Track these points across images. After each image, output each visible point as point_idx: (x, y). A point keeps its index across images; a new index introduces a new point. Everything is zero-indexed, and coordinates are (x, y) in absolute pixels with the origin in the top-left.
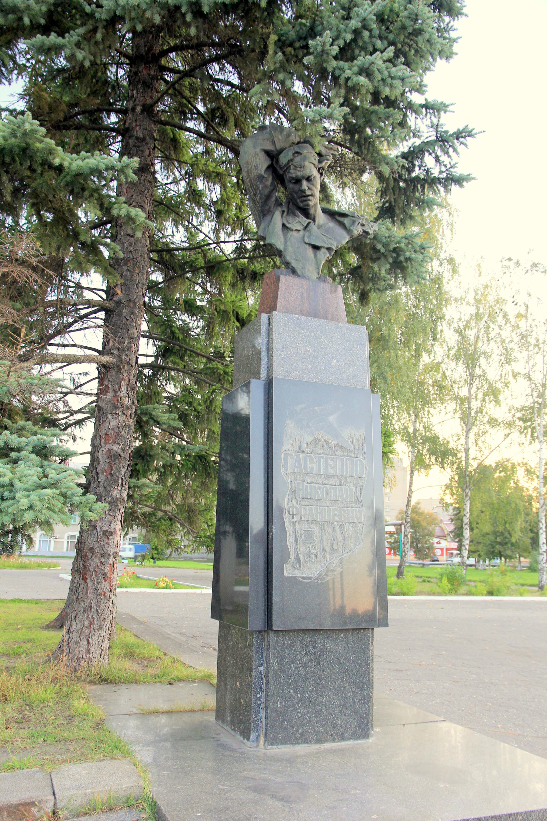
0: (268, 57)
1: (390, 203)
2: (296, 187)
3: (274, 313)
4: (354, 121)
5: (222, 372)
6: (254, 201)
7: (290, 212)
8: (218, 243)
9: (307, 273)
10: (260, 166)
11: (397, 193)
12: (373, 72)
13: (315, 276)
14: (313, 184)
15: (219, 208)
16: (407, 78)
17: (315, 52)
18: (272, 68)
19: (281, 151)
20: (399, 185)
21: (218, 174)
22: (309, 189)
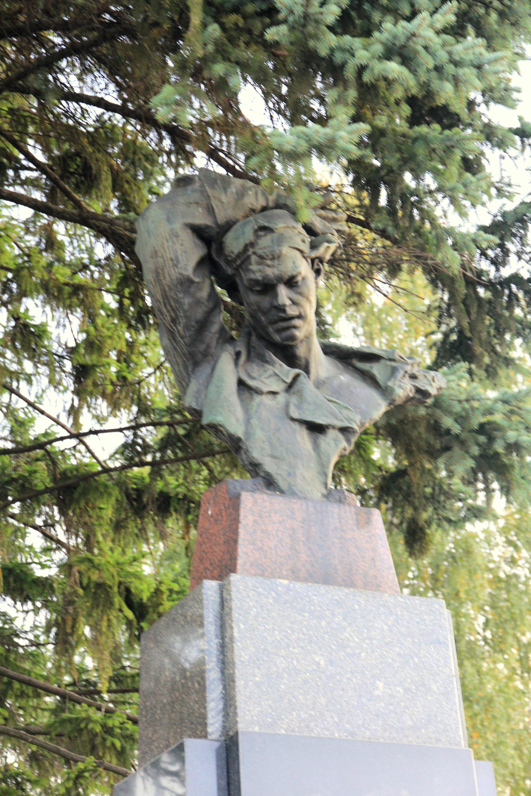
0: (190, 34)
1: (461, 333)
2: (265, 302)
3: (234, 577)
4: (377, 163)
5: (98, 729)
6: (172, 335)
7: (254, 356)
8: (79, 436)
9: (300, 484)
10: (183, 259)
11: (474, 310)
12: (416, 52)
13: (317, 491)
14: (301, 294)
15: (82, 361)
16: (489, 63)
17: (291, 19)
18: (200, 53)
19: (229, 226)
20: (476, 293)
21: (77, 289)
22: (294, 303)
